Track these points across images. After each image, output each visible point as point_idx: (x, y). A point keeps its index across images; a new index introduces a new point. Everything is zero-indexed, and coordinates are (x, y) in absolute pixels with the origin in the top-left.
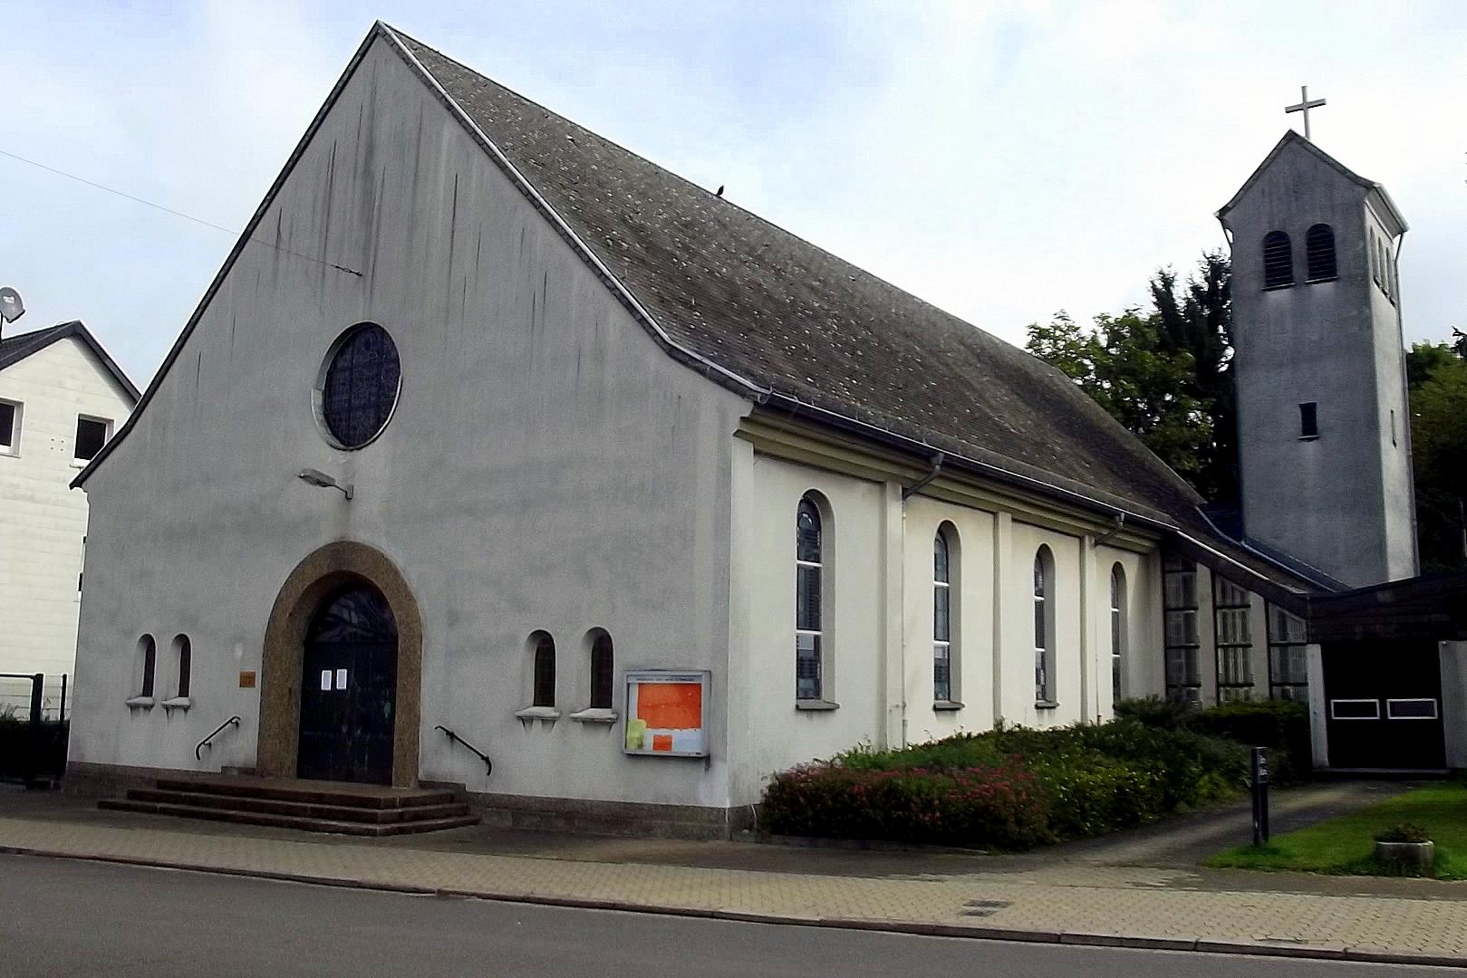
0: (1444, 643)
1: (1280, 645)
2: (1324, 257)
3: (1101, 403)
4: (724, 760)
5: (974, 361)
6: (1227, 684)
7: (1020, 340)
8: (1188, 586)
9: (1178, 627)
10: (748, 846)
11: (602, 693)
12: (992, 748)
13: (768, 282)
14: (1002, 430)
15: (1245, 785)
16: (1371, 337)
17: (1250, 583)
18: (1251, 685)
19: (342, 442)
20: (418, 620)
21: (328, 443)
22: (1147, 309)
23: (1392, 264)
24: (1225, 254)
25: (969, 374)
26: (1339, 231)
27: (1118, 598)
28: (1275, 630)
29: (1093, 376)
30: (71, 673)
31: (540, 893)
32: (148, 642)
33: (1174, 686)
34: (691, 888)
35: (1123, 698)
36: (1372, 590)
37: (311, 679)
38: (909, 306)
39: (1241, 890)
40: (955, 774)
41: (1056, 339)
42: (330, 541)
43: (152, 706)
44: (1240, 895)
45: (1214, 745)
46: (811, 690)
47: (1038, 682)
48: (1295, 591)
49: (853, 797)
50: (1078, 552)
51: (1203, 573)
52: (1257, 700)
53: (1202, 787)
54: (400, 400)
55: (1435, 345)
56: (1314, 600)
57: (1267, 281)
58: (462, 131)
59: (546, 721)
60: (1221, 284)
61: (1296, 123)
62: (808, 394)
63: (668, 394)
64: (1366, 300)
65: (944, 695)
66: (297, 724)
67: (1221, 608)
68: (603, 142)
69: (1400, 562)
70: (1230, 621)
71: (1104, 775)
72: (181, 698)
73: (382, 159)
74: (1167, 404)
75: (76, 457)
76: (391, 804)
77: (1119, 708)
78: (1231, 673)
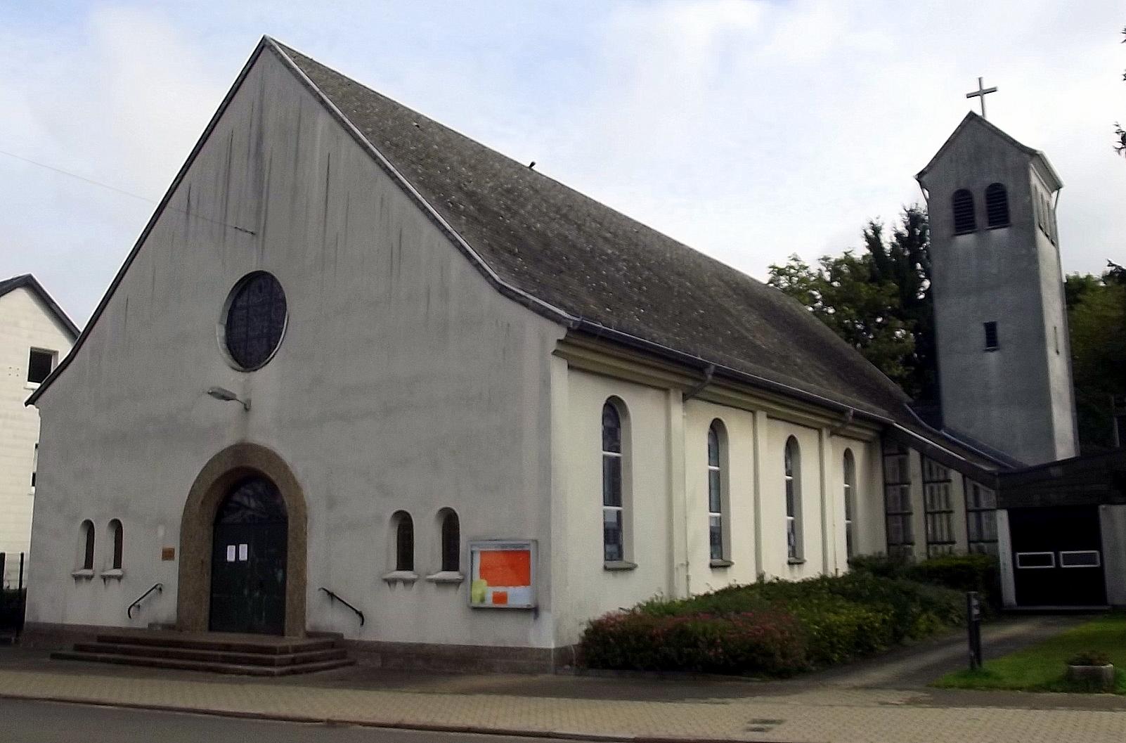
0: (1104, 506)
1: (975, 510)
2: (1001, 209)
3: (829, 324)
4: (549, 610)
5: (730, 293)
6: (935, 543)
7: (764, 277)
8: (903, 466)
9: (895, 498)
10: (570, 679)
11: (451, 559)
12: (758, 597)
13: (572, 234)
14: (755, 347)
15: (954, 622)
16: (1038, 269)
17: (950, 463)
18: (953, 543)
19: (241, 365)
20: (304, 505)
21: (229, 366)
22: (860, 250)
23: (1052, 213)
24: (922, 206)
25: (728, 304)
26: (1011, 187)
27: (849, 477)
28: (971, 498)
29: (820, 304)
30: (27, 551)
31: (409, 720)
32: (89, 527)
33: (894, 545)
34: (529, 713)
35: (855, 555)
36: (1045, 467)
37: (219, 553)
38: (680, 252)
39: (965, 705)
40: (732, 618)
41: (791, 276)
42: (232, 443)
43: (92, 577)
44: (965, 711)
45: (929, 591)
46: (615, 553)
47: (789, 544)
48: (986, 468)
49: (652, 638)
50: (817, 441)
51: (914, 455)
52: (959, 555)
53: (922, 623)
54: (288, 331)
55: (1082, 275)
56: (1001, 475)
57: (957, 228)
58: (333, 120)
59: (407, 582)
60: (918, 232)
61: (974, 106)
62: (607, 322)
63: (499, 322)
64: (1033, 242)
65: (718, 555)
66: (208, 589)
67: (929, 482)
68: (442, 128)
69: (1065, 446)
70: (936, 492)
71: (846, 616)
72: (116, 570)
73: (270, 144)
74: (879, 326)
75: (29, 381)
76: (285, 651)
77: (854, 562)
78: (938, 533)
